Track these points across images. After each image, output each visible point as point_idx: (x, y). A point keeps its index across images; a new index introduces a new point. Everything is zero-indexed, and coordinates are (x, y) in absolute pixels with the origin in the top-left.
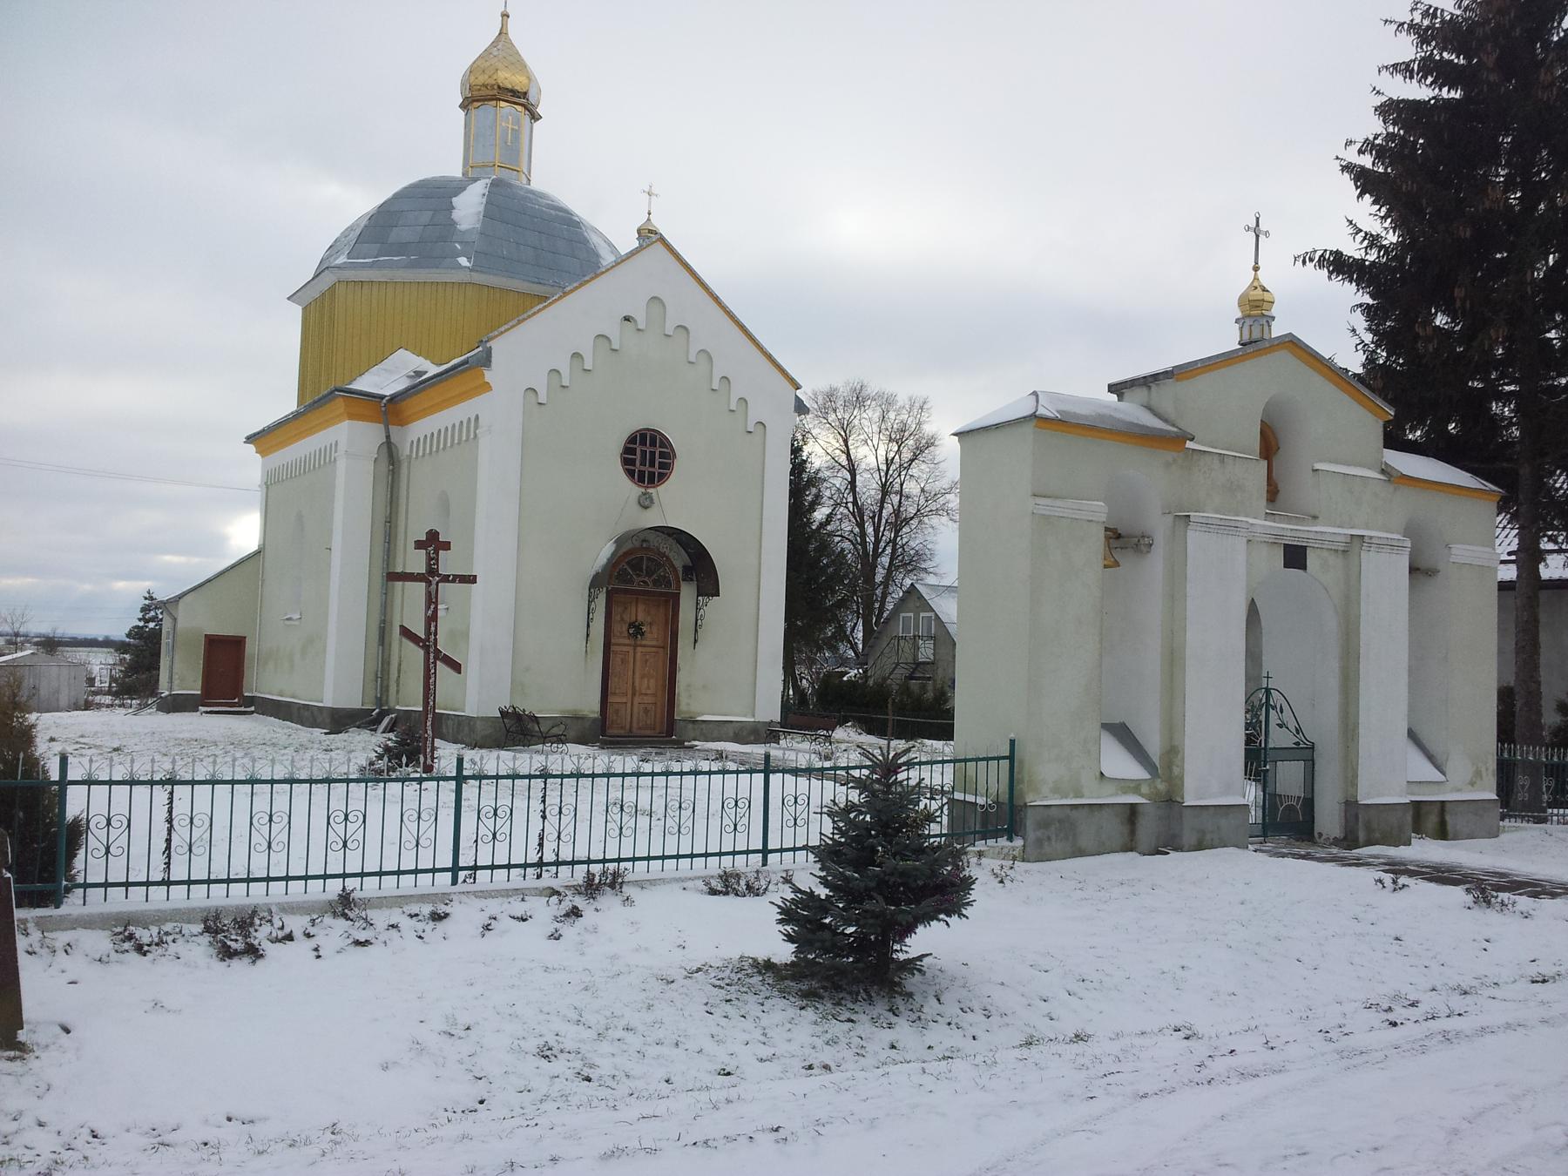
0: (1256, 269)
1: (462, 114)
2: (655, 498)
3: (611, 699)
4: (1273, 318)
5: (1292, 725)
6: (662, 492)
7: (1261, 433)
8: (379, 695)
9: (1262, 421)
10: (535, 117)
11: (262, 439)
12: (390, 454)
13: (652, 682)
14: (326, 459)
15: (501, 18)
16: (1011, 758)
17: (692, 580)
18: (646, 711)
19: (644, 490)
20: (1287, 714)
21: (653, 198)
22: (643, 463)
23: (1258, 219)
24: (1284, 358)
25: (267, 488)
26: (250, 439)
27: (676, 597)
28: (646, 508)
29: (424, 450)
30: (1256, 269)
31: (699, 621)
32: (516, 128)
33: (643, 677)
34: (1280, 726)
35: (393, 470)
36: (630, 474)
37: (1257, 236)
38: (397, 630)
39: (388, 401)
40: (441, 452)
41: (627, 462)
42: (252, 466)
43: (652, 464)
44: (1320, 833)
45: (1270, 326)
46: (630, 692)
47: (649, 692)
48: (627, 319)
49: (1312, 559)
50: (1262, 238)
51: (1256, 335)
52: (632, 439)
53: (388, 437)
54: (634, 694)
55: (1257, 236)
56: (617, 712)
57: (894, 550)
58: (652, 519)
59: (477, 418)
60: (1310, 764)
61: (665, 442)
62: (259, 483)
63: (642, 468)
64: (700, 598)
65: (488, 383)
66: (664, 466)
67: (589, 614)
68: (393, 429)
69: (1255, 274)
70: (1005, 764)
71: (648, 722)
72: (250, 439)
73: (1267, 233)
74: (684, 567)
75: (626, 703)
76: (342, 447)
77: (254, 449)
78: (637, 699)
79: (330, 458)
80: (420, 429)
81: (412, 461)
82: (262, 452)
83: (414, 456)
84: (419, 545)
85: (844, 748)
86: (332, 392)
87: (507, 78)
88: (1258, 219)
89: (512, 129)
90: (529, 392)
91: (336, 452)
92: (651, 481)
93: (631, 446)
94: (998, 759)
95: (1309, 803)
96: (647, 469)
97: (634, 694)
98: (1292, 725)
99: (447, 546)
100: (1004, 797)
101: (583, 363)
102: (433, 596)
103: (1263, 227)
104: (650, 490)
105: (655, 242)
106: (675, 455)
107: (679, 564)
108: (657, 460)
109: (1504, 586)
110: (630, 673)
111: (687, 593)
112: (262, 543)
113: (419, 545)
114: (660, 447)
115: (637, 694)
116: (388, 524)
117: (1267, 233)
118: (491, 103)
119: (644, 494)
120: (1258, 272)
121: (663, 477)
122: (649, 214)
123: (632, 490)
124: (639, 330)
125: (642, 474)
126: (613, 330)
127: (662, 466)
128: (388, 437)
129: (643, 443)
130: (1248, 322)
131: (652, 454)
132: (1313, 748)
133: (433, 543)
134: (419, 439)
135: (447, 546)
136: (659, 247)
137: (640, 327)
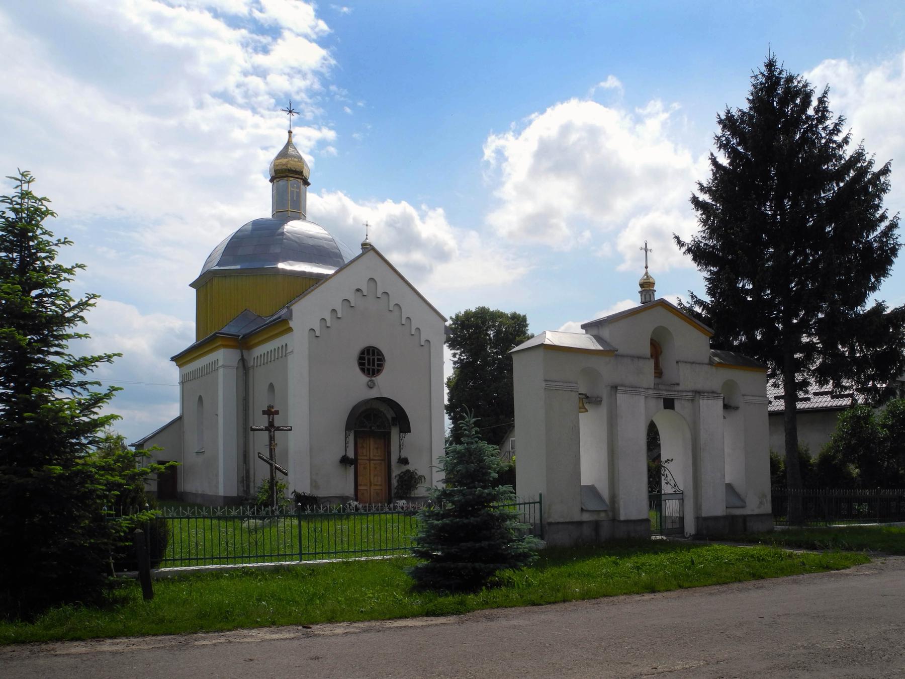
0: (646, 267)
1: (271, 184)
2: (375, 381)
3: (359, 488)
4: (655, 291)
5: (672, 483)
6: (380, 379)
7: (651, 344)
8: (245, 489)
9: (651, 340)
10: (306, 183)
11: (180, 359)
12: (244, 367)
13: (380, 479)
14: (212, 368)
15: (288, 134)
16: (540, 502)
17: (396, 425)
18: (377, 494)
19: (370, 379)
20: (669, 477)
21: (368, 227)
22: (369, 364)
23: (646, 244)
24: (660, 309)
25: (183, 384)
26: (174, 359)
27: (389, 434)
28: (371, 388)
29: (261, 362)
30: (646, 267)
31: (401, 446)
32: (298, 190)
33: (375, 476)
34: (667, 483)
35: (245, 373)
36: (363, 370)
37: (646, 252)
38: (257, 455)
39: (242, 338)
40: (269, 363)
41: (361, 365)
42: (174, 373)
43: (374, 365)
44: (687, 533)
45: (654, 295)
46: (369, 485)
47: (378, 484)
48: (358, 290)
49: (677, 404)
50: (649, 252)
51: (648, 299)
52: (363, 352)
53: (242, 356)
54: (371, 485)
55: (646, 252)
56: (363, 494)
57: (87, 456)
58: (374, 394)
59: (286, 345)
60: (682, 500)
61: (379, 353)
62: (178, 381)
63: (369, 367)
64: (401, 434)
65: (291, 327)
66: (379, 365)
67: (346, 444)
68: (245, 352)
69: (647, 270)
70: (537, 505)
71: (379, 499)
72: (174, 359)
73: (651, 250)
74: (392, 418)
75: (367, 490)
76: (220, 363)
77: (175, 364)
78: (372, 487)
79: (215, 367)
80: (260, 350)
81: (255, 368)
82: (179, 366)
83: (256, 365)
84: (264, 412)
85: (621, 639)
86: (214, 335)
87: (292, 164)
88: (646, 244)
89: (296, 191)
90: (311, 331)
91: (217, 365)
92: (373, 374)
93: (363, 356)
94: (534, 503)
95: (682, 519)
96: (371, 367)
97: (371, 485)
98: (672, 483)
99: (277, 412)
100: (538, 522)
101: (337, 314)
102: (272, 438)
103: (649, 247)
104: (373, 379)
105: (370, 250)
106: (385, 360)
107: (389, 417)
108: (376, 362)
109: (773, 415)
110: (368, 475)
111: (395, 433)
112: (182, 412)
113: (264, 412)
114: (377, 355)
115: (372, 485)
116: (244, 401)
117: (651, 250)
118: (285, 179)
119: (370, 381)
120: (648, 269)
121: (379, 371)
122: (367, 235)
123: (364, 379)
124: (364, 296)
125: (369, 370)
126: (351, 297)
127: (379, 360)
128: (242, 356)
129: (368, 354)
130: (644, 293)
131: (374, 360)
132: (683, 493)
133: (270, 412)
134: (258, 357)
135: (277, 412)
136: (372, 252)
137: (364, 294)
